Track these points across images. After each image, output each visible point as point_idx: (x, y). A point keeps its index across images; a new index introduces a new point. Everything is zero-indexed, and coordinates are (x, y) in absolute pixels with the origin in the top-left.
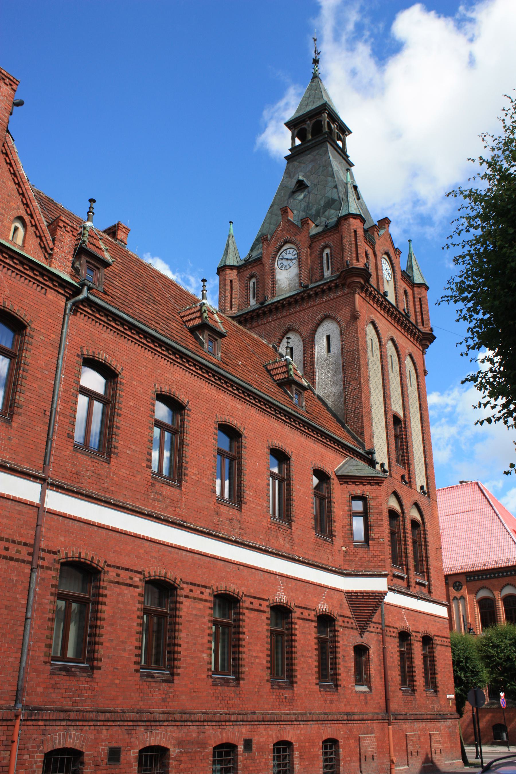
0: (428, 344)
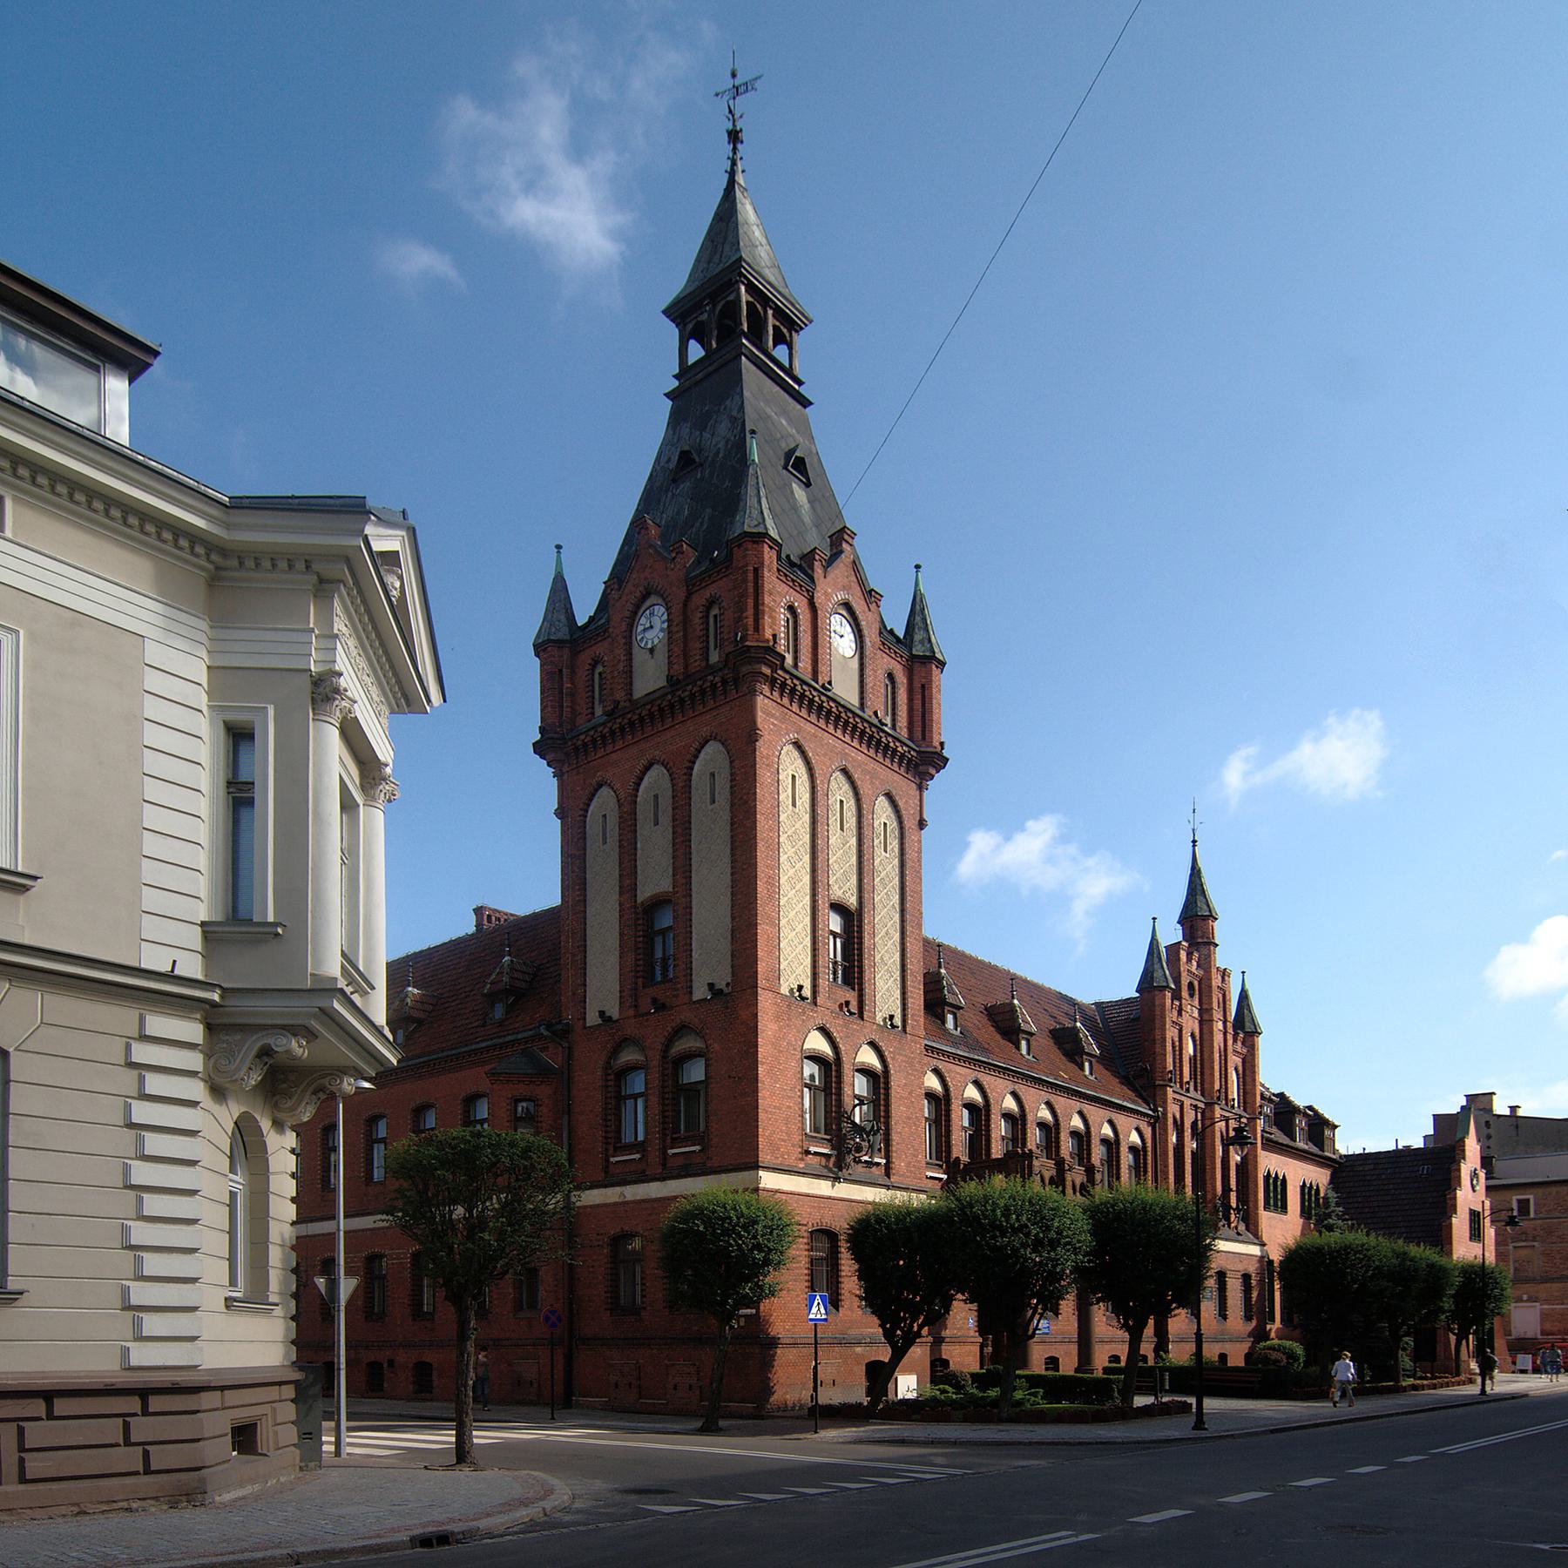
0: (932, 771)
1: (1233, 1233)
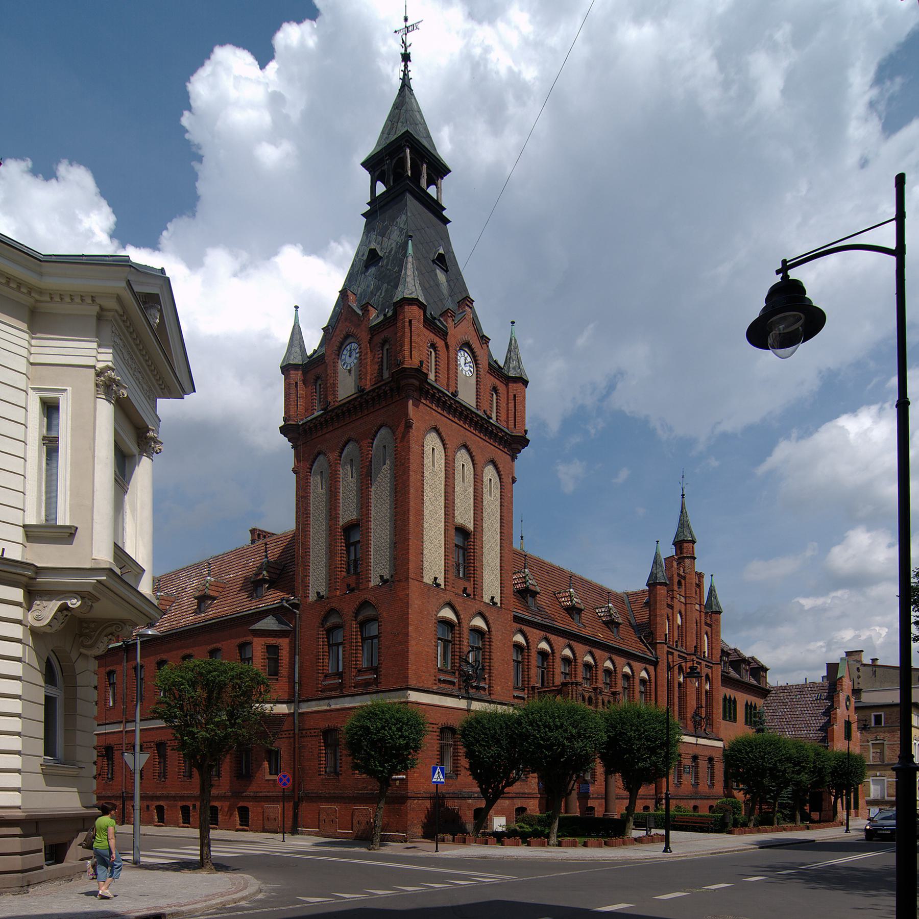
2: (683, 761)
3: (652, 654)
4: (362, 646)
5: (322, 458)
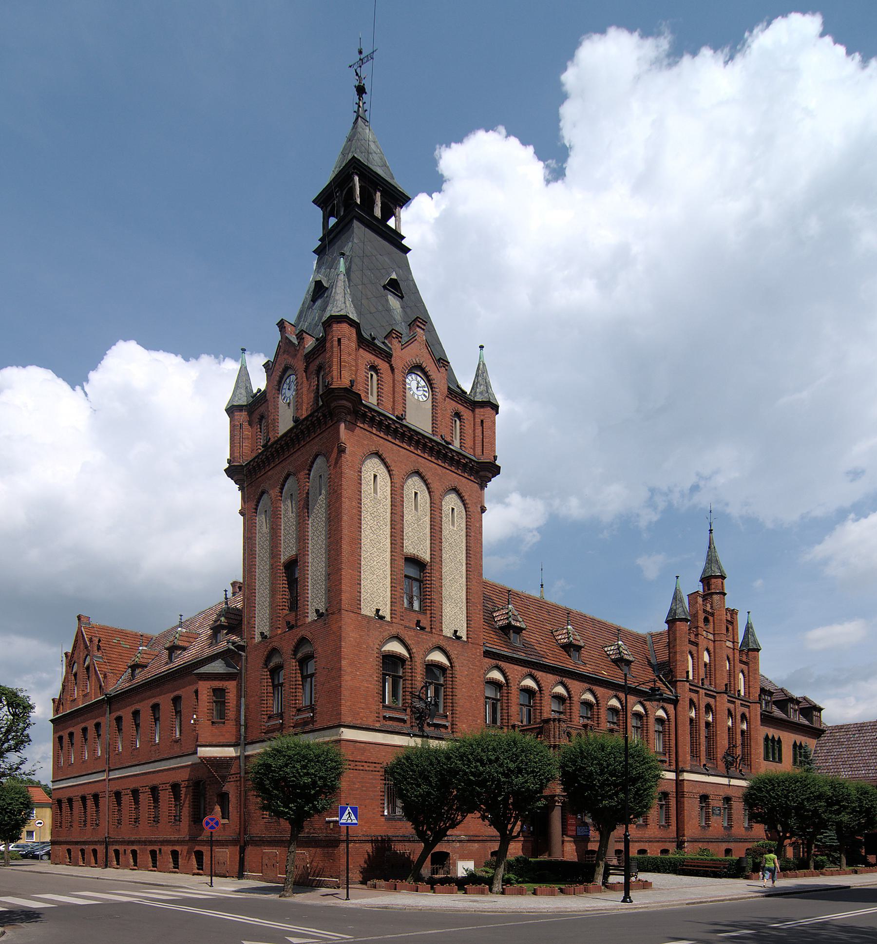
1: (737, 774)
2: (712, 803)
3: (671, 691)
4: (302, 685)
5: (266, 497)
